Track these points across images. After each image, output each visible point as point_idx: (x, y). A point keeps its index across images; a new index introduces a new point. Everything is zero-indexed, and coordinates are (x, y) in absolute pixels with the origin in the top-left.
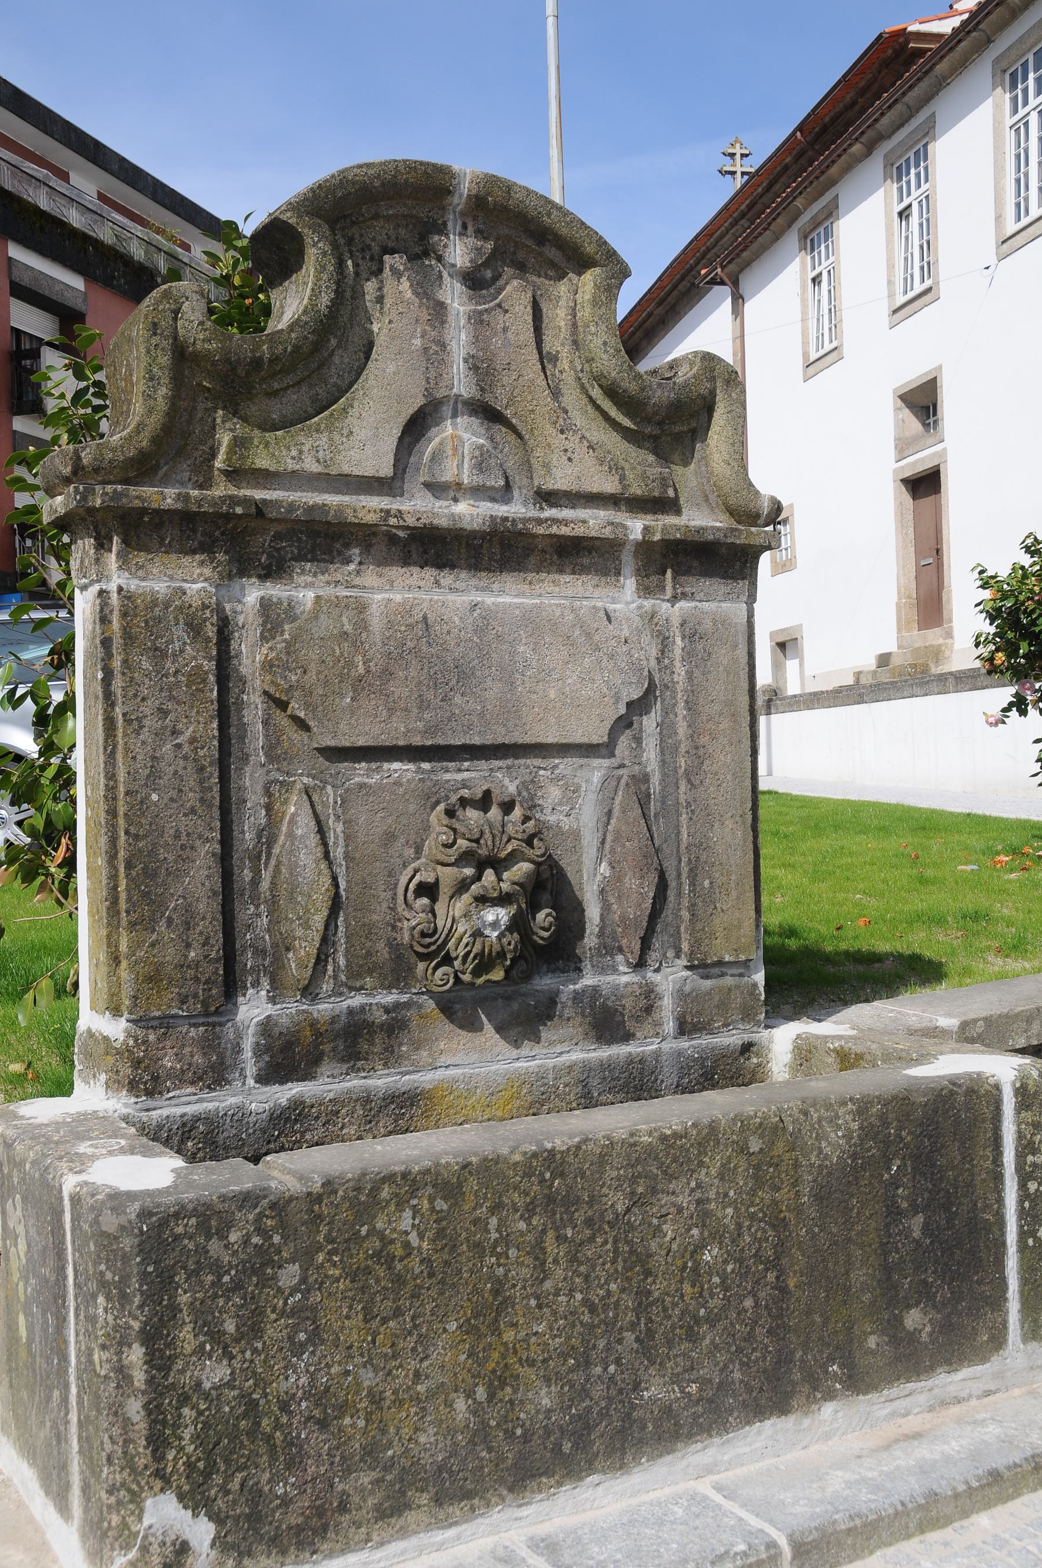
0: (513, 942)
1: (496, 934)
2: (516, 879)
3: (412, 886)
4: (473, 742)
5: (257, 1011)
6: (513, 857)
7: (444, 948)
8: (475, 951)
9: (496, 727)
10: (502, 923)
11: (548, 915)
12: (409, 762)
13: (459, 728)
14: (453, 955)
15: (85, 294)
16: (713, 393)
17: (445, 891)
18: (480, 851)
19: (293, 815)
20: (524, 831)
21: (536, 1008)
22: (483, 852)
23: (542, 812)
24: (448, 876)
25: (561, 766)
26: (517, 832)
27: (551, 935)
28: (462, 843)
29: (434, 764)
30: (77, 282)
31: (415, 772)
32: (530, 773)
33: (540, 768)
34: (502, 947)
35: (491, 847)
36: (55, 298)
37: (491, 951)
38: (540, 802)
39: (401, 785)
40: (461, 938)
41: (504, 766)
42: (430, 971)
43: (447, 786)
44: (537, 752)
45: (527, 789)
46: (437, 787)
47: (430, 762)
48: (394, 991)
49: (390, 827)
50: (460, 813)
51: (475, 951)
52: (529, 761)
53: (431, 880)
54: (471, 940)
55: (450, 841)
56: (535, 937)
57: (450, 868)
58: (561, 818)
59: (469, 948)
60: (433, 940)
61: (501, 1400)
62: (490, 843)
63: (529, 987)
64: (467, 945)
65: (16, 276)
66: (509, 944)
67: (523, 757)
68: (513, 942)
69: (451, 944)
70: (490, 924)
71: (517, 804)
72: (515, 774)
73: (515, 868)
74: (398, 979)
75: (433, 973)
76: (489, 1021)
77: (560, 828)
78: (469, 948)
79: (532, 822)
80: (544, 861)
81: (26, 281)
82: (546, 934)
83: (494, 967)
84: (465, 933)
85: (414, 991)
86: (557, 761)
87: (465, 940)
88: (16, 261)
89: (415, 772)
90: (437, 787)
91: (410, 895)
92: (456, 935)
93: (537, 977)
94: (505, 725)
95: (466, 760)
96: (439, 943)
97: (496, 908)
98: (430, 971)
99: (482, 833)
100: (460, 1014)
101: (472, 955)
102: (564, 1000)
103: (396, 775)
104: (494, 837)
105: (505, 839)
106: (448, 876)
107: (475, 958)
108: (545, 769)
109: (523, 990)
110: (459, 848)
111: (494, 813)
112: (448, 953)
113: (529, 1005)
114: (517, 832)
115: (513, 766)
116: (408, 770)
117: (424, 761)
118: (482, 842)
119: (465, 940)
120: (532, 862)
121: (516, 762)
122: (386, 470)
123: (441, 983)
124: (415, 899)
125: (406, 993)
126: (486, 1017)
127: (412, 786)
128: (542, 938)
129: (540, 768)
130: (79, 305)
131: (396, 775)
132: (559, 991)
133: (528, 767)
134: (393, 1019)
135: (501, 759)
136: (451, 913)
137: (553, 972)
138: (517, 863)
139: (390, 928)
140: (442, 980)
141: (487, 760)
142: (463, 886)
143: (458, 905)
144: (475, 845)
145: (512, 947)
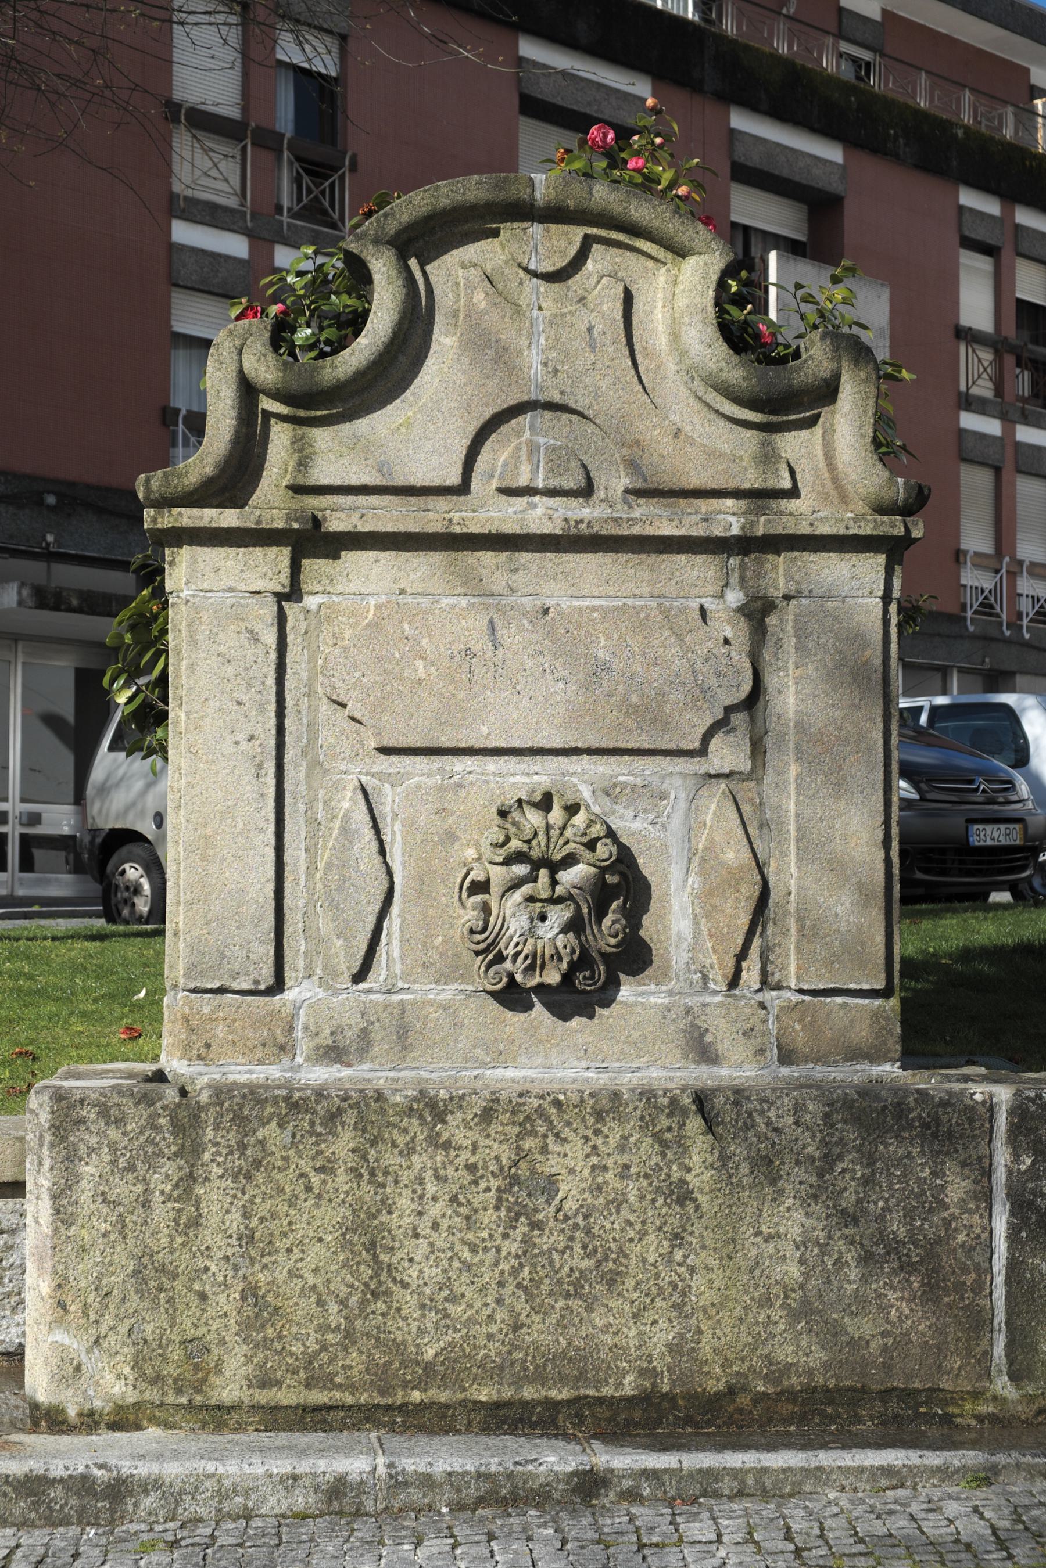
3: (466, 884)
5: (308, 995)
6: (570, 860)
11: (614, 922)
14: (505, 953)
15: (844, 167)
16: (837, 377)
17: (495, 889)
19: (347, 811)
22: (535, 853)
24: (498, 875)
28: (515, 844)
30: (832, 153)
36: (797, 178)
40: (511, 938)
42: (483, 969)
50: (516, 815)
51: (525, 951)
53: (481, 878)
55: (501, 841)
59: (519, 948)
61: (373, 1312)
62: (543, 844)
64: (517, 944)
65: (740, 156)
69: (502, 945)
71: (583, 808)
78: (519, 948)
81: (755, 159)
82: (613, 941)
87: (515, 940)
88: (740, 132)
91: (465, 894)
96: (490, 940)
99: (536, 834)
101: (522, 956)
104: (549, 839)
105: (561, 842)
106: (498, 875)
107: (526, 958)
111: (556, 815)
112: (500, 951)
119: (515, 940)
122: (454, 478)
124: (469, 896)
130: (835, 186)
142: (515, 885)
144: (525, 845)
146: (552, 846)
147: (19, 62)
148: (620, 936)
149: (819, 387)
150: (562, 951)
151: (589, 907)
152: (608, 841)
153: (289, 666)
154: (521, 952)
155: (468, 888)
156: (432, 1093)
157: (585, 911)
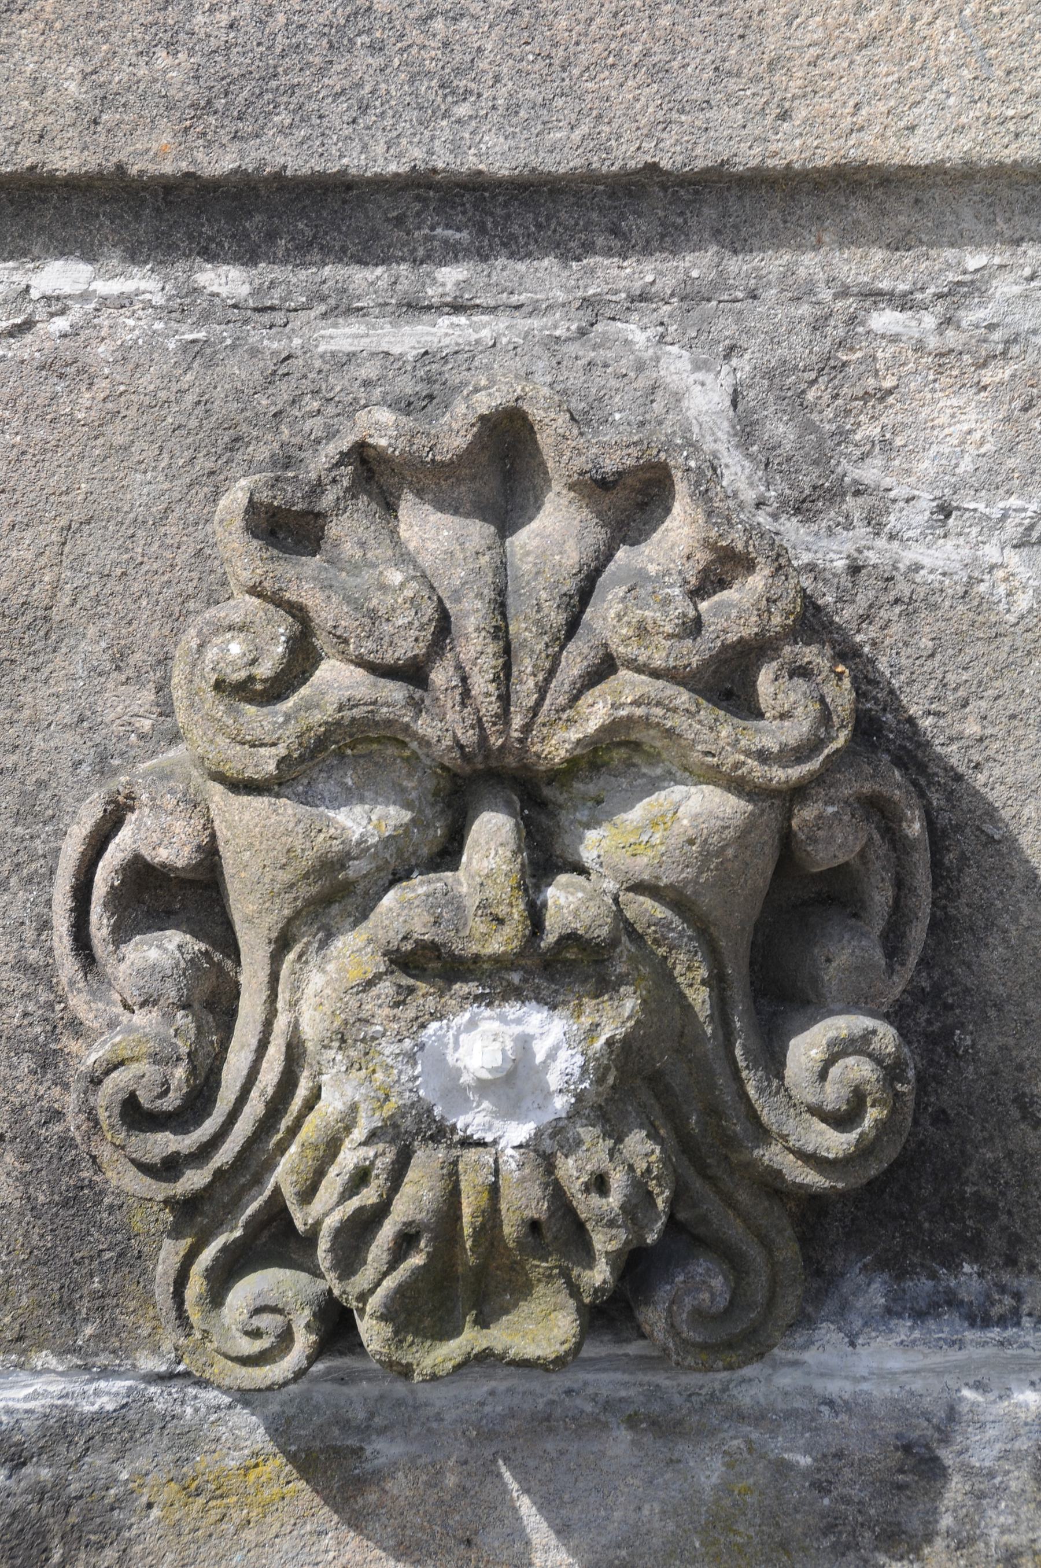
0: (618, 1180)
1: (519, 1132)
2: (642, 866)
4: (471, 162)
7: (258, 1180)
8: (401, 1211)
9: (608, 81)
10: (554, 1080)
11: (838, 1050)
12: (133, 256)
13: (396, 87)
18: (425, 726)
20: (694, 627)
21: (821, 1488)
23: (874, 521)
25: (1005, 288)
26: (642, 630)
27: (864, 1151)
29: (266, 272)
31: (166, 312)
32: (818, 325)
33: (874, 297)
34: (558, 1195)
35: (489, 707)
37: (492, 1214)
38: (869, 473)
39: (87, 376)
40: (332, 1147)
41: (667, 284)
42: (196, 1286)
43: (337, 384)
44: (860, 210)
45: (798, 402)
46: (284, 391)
47: (249, 257)
48: (43, 1358)
49: (30, 578)
51: (401, 1211)
52: (809, 264)
54: (384, 1156)
55: (265, 669)
56: (774, 1156)
57: (260, 803)
58: (991, 553)
59: (369, 1196)
60: (186, 1143)
62: (482, 684)
63: (786, 1379)
64: (361, 1177)
66: (600, 1184)
67: (776, 240)
68: (618, 1180)
70: (483, 1087)
71: (681, 487)
72: (726, 328)
73: (638, 813)
74: (66, 1306)
75: (216, 1297)
76: (563, 1530)
77: (983, 605)
79: (757, 581)
80: (818, 779)
83: (523, 1290)
84: (348, 1120)
85: (149, 1363)
86: (975, 260)
87: (349, 1158)
89: (166, 312)
90: (284, 391)
91: (99, 922)
92: (312, 1129)
93: (828, 1333)
94: (659, 72)
95: (453, 253)
96: (225, 1155)
97: (512, 1010)
98: (196, 1286)
100: (399, 1486)
101: (387, 1232)
102: (982, 1457)
103: (61, 324)
107: (406, 1242)
108: (904, 302)
109: (746, 1397)
110: (309, 706)
113: (782, 1468)
114: (642, 630)
115: (720, 283)
116: (124, 302)
117: (210, 255)
118: (441, 676)
119: (349, 1158)
120: (737, 785)
121: (734, 265)
123: (249, 1347)
124: (121, 934)
125: (105, 1373)
126: (545, 1505)
127: (147, 381)
128: (812, 1159)
129: (874, 297)
131: (61, 324)
132: (952, 1414)
133: (805, 292)
134: (40, 1493)
135: (647, 250)
136: (281, 1023)
137: (920, 1315)
138: (654, 785)
139: (26, 1063)
140: (255, 1334)
141: (566, 256)
143: (316, 981)
144: (395, 692)
145: (614, 1200)
146: (525, 688)
147: (978, 639)
148: (873, 1115)
149: (756, 242)
150: (588, 1205)
151: (717, 982)
152: (810, 654)
153: (317, 165)
154: (381, 1211)
155: (116, 899)
156: (198, 1374)
157: (699, 998)
